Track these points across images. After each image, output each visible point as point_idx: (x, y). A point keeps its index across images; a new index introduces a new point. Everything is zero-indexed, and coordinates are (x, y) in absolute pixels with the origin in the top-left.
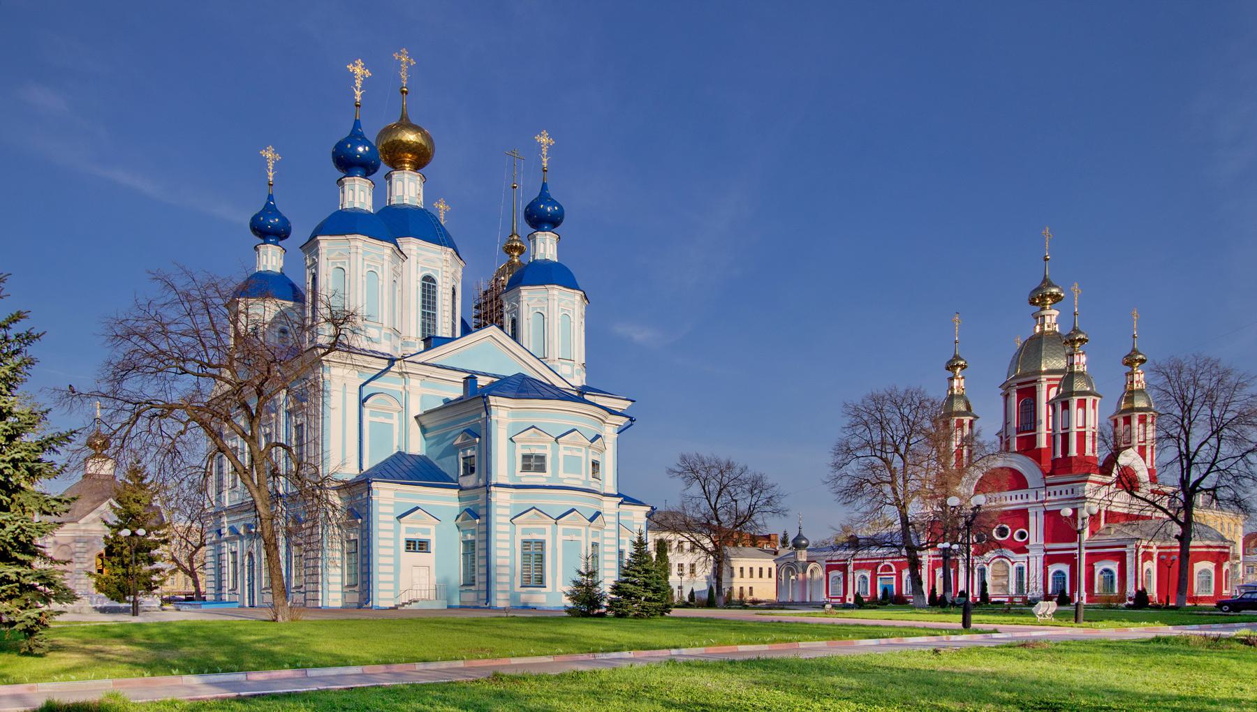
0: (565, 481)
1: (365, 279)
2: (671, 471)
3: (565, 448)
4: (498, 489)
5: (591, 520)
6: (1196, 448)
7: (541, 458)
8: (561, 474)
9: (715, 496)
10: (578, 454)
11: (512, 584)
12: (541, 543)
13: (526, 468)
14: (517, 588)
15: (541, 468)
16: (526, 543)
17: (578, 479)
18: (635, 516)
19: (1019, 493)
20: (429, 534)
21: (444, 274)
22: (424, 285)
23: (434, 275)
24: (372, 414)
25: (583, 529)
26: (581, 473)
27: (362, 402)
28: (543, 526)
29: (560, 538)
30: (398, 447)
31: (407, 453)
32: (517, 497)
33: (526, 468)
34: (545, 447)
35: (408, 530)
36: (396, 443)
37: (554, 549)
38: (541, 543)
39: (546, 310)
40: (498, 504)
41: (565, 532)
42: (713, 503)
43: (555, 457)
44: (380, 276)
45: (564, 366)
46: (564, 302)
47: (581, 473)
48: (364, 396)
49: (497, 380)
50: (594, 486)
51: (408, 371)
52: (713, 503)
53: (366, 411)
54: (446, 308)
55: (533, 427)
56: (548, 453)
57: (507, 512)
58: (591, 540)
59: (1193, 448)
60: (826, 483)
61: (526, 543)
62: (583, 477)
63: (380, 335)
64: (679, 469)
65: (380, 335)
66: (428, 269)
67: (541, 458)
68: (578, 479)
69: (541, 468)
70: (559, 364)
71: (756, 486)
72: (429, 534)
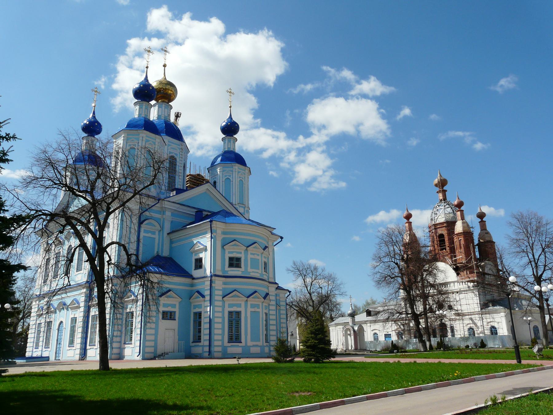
0: (251, 274)
1: (224, 183)
2: (288, 270)
4: (217, 278)
5: (265, 298)
6: (538, 257)
7: (239, 259)
8: (249, 269)
9: (310, 287)
11: (222, 340)
12: (238, 313)
13: (231, 265)
14: (226, 344)
15: (238, 266)
16: (230, 313)
17: (258, 273)
18: (280, 296)
19: (472, 275)
20: (240, 307)
21: (180, 156)
24: (145, 231)
25: (261, 304)
26: (259, 269)
27: (140, 223)
28: (240, 302)
29: (249, 309)
30: (157, 252)
31: (162, 256)
32: (225, 283)
33: (231, 265)
34: (241, 253)
35: (230, 306)
36: (156, 251)
37: (246, 317)
38: (238, 313)
39: (231, 176)
40: (216, 288)
41: (253, 306)
42: (309, 289)
43: (246, 259)
44: (231, 180)
45: (240, 208)
46: (241, 173)
47: (259, 269)
48: (142, 219)
49: (210, 214)
50: (265, 277)
51: (166, 206)
52: (309, 289)
53: (142, 230)
54: (181, 171)
55: (235, 240)
56: (242, 256)
57: (220, 293)
58: (265, 311)
59: (536, 257)
60: (369, 276)
61: (230, 313)
62: (260, 271)
63: (244, 211)
64: (292, 269)
65: (244, 211)
67: (239, 259)
69: (238, 266)
70: (238, 207)
71: (330, 278)
72: (240, 307)
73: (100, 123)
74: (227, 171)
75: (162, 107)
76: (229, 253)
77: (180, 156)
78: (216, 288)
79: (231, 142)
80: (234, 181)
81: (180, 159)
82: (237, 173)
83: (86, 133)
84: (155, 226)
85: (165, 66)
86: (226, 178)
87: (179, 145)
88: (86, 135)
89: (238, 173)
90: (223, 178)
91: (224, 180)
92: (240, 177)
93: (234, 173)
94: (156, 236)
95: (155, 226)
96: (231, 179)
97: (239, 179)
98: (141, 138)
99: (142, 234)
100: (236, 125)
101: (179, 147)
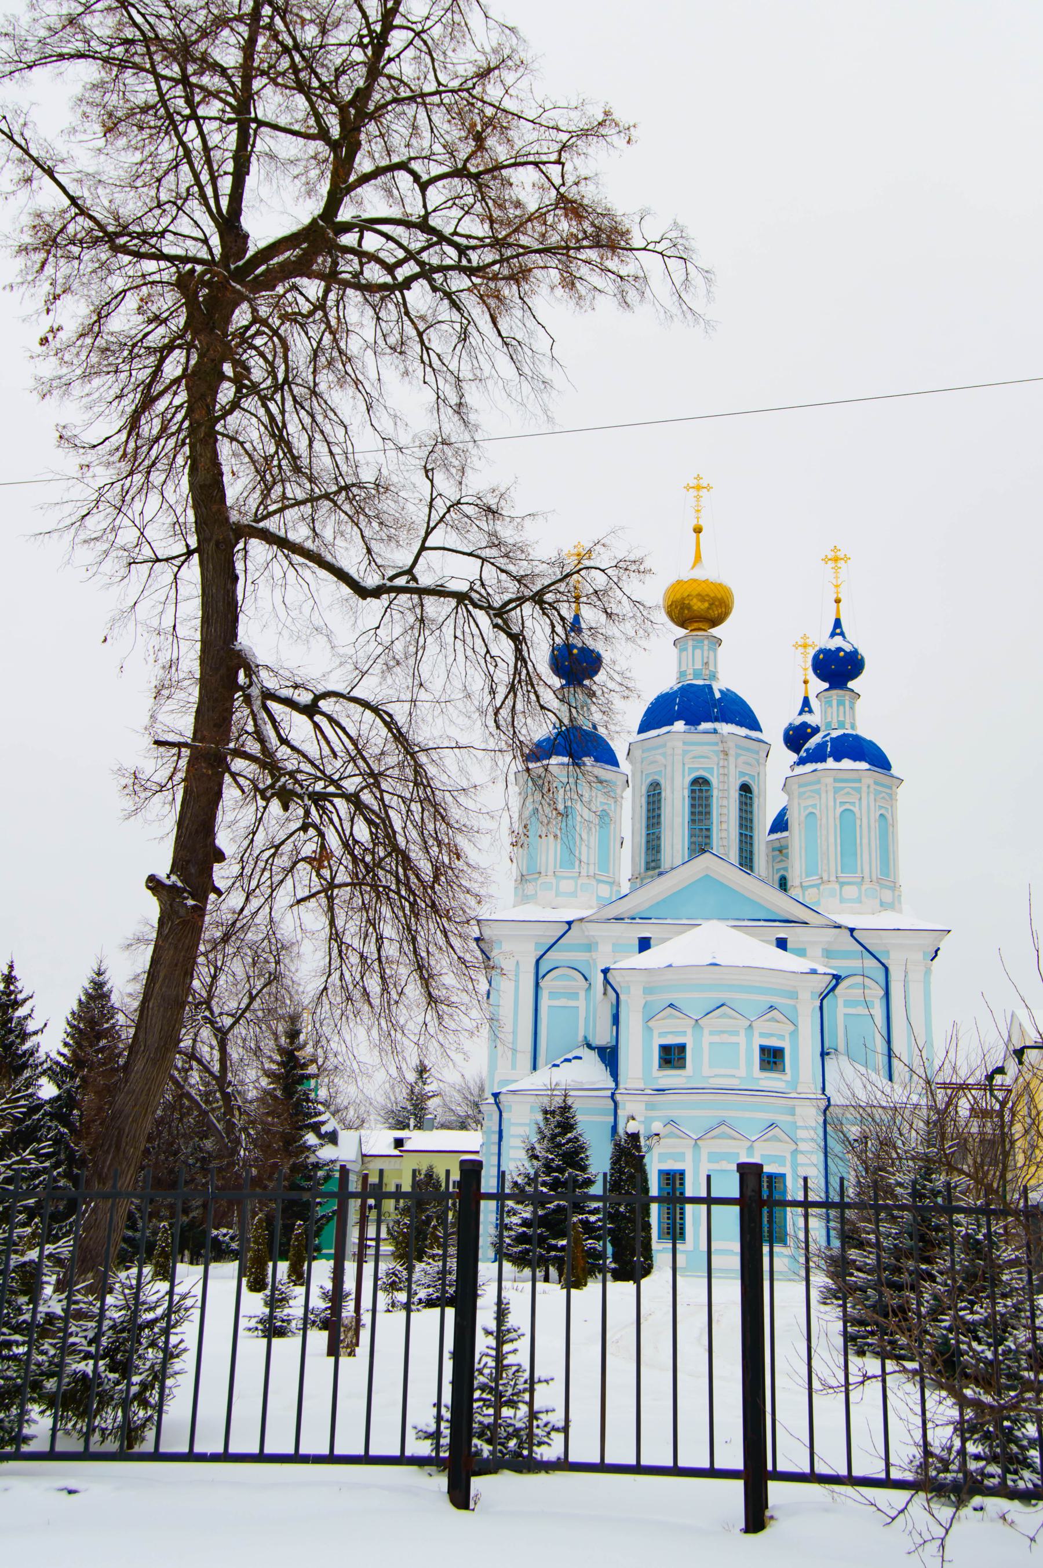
3: (712, 1033)
8: (706, 1071)
10: (734, 1039)
21: (721, 771)
22: (693, 791)
23: (656, 777)
24: (553, 995)
40: (513, 1121)
44: (858, 815)
56: (687, 1040)
62: (742, 1072)
66: (698, 769)
68: (734, 1076)
73: (655, 696)
74: (846, 790)
75: (686, 649)
76: (762, 1035)
77: (721, 771)
78: (513, 1121)
79: (844, 706)
80: (824, 821)
81: (722, 778)
82: (831, 795)
83: (824, 680)
84: (575, 980)
85: (698, 530)
86: (807, 812)
87: (717, 744)
88: (826, 685)
89: (835, 793)
90: (835, 809)
91: (803, 818)
92: (881, 807)
93: (823, 795)
94: (581, 1003)
95: (575, 980)
96: (856, 809)
97: (839, 810)
98: (864, 789)
99: (545, 1003)
100: (821, 656)
101: (716, 748)
